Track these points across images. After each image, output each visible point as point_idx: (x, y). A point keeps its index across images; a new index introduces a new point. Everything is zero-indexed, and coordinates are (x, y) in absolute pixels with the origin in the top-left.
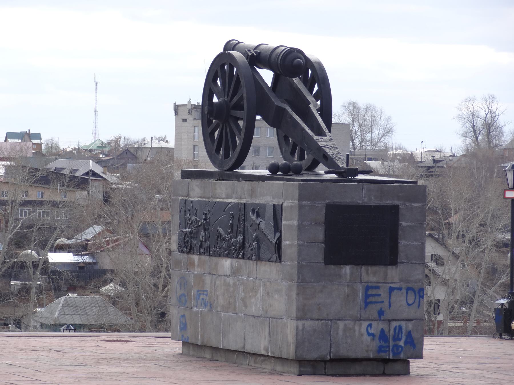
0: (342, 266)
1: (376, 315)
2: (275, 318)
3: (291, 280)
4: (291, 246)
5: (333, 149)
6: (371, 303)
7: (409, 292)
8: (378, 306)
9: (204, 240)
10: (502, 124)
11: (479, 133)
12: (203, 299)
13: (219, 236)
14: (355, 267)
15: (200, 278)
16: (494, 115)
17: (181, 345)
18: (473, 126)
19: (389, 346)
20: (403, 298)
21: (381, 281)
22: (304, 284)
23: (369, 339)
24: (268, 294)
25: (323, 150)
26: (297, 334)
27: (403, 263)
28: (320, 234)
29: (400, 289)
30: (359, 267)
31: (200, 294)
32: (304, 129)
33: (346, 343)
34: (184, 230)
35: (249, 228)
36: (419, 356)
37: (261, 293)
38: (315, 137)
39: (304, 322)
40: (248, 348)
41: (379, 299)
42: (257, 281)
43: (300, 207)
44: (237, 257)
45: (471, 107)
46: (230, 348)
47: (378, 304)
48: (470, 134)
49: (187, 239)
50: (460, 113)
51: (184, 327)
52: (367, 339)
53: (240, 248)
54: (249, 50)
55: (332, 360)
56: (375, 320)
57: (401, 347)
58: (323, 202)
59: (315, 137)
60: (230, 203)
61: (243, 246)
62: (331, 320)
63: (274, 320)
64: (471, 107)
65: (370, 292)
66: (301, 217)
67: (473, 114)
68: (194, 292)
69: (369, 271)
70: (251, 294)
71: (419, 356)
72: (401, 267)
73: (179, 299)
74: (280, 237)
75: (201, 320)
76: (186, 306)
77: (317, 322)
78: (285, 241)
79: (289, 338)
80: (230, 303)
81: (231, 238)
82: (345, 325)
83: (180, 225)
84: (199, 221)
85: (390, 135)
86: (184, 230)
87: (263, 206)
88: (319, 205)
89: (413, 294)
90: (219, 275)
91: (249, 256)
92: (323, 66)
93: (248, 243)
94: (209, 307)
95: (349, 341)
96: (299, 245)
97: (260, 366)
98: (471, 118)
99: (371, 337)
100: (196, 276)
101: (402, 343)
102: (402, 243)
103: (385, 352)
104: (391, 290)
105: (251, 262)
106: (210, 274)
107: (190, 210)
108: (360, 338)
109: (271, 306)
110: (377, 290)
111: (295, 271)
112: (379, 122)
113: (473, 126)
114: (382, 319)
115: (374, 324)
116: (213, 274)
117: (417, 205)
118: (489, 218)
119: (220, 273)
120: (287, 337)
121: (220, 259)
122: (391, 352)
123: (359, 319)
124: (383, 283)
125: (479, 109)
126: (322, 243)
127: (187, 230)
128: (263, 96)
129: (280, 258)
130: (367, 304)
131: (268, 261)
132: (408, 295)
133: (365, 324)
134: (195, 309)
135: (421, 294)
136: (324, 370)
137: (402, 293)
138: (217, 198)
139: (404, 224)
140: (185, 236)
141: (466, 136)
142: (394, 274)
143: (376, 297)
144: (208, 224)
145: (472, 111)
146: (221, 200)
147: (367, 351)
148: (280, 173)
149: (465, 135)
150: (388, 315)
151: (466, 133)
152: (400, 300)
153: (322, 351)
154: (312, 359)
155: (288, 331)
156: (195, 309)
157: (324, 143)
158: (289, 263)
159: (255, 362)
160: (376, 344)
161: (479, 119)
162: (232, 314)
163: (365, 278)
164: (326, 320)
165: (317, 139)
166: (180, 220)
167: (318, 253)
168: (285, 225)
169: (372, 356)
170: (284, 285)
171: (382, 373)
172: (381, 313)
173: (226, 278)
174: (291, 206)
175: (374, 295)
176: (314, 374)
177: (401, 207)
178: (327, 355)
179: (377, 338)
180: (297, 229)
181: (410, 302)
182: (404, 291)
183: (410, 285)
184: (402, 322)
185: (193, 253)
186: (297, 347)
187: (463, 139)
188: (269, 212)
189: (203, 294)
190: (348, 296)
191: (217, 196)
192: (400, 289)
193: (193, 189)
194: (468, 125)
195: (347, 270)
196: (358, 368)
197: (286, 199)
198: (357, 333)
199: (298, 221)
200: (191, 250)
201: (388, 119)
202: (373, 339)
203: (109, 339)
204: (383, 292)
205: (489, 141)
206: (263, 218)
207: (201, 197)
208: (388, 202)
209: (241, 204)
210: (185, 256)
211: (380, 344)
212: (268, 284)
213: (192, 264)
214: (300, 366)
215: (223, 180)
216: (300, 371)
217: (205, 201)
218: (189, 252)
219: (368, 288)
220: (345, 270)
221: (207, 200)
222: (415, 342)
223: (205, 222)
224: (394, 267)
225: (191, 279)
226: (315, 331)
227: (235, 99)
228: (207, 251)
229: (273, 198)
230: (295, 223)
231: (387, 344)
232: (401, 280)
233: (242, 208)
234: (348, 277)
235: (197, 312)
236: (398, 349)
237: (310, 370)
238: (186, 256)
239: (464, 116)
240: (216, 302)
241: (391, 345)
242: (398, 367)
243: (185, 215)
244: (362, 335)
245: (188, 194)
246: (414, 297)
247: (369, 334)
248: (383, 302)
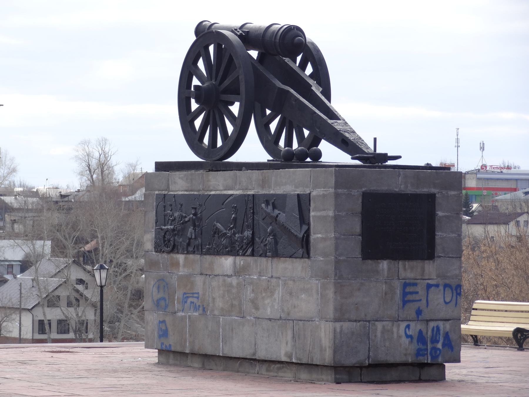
0: (379, 261)
1: (413, 315)
2: (301, 320)
3: (326, 277)
4: (324, 239)
5: (352, 134)
6: (409, 301)
7: (447, 289)
8: (416, 305)
9: (193, 237)
10: (114, 163)
11: (94, 172)
12: (192, 302)
13: (217, 231)
14: (393, 262)
15: (187, 279)
16: (107, 155)
17: (157, 354)
18: (89, 166)
19: (427, 349)
20: (441, 296)
21: (418, 277)
22: (341, 281)
23: (407, 341)
24: (291, 294)
25: (342, 134)
26: (335, 337)
27: (440, 257)
28: (356, 225)
29: (437, 286)
30: (396, 262)
31: (188, 297)
32: (315, 113)
33: (385, 346)
34: (163, 227)
35: (261, 222)
36: (457, 360)
37: (279, 293)
38: (330, 121)
39: (342, 323)
40: (261, 354)
41: (416, 297)
42: (274, 280)
43: (337, 196)
44: (244, 255)
45: (86, 148)
46: (234, 355)
47: (415, 303)
48: (86, 172)
49: (167, 237)
50: (77, 154)
51: (164, 334)
52: (405, 341)
53: (248, 244)
54: (236, 30)
55: (370, 366)
56: (413, 321)
57: (439, 349)
58: (360, 190)
59: (330, 121)
60: (232, 195)
61: (252, 242)
62: (369, 321)
63: (301, 323)
64: (86, 148)
65: (408, 290)
66: (338, 207)
67: (88, 155)
68: (179, 294)
69: (407, 266)
70: (264, 295)
71: (457, 360)
72: (438, 261)
73: (157, 304)
74: (309, 229)
75: (190, 326)
76: (168, 310)
77: (355, 323)
78: (314, 234)
79: (323, 342)
80: (232, 305)
81: (234, 234)
82: (384, 327)
83: (156, 223)
84: (185, 217)
85: (14, 174)
86: (163, 227)
87: (284, 197)
88: (356, 194)
89: (450, 291)
90: (216, 276)
91: (261, 252)
92: (317, 47)
93: (259, 238)
94: (201, 311)
95: (387, 344)
96: (336, 238)
97: (275, 374)
98: (87, 159)
99: (410, 339)
100: (180, 278)
101: (439, 346)
102: (439, 234)
103: (423, 355)
104: (429, 286)
105: (264, 260)
106: (201, 274)
107: (171, 205)
108: (398, 341)
109: (295, 307)
110: (415, 287)
111: (331, 268)
112: (3, 163)
113: (89, 166)
114: (420, 319)
115: (412, 324)
116: (206, 275)
117: (453, 193)
118: (135, 245)
119: (216, 273)
120: (320, 341)
121: (218, 257)
122: (429, 355)
123: (397, 320)
124: (421, 279)
125: (94, 150)
126: (359, 235)
127: (169, 227)
128: (256, 78)
129: (308, 253)
130: (405, 302)
131: (291, 257)
132: (446, 293)
133: (403, 325)
134: (180, 314)
135: (459, 291)
136: (360, 377)
137: (440, 291)
138: (211, 191)
139: (440, 213)
140: (165, 234)
141: (82, 175)
142: (430, 269)
143: (414, 295)
144: (200, 219)
145: (88, 152)
146: (218, 192)
147: (405, 355)
148: (308, 160)
149: (82, 174)
150: (426, 315)
151: (82, 172)
152: (437, 297)
153: (360, 357)
154: (351, 365)
155: (323, 335)
156: (180, 314)
157: (341, 127)
158: (322, 259)
159: (268, 370)
160: (414, 347)
161: (94, 159)
162: (236, 318)
163: (402, 274)
164: (364, 321)
165: (332, 123)
166: (156, 216)
167: (355, 246)
168: (314, 216)
169: (410, 361)
170: (315, 283)
171: (418, 378)
172: (419, 312)
173: (226, 278)
174: (323, 194)
175: (411, 293)
176: (350, 381)
177: (437, 195)
178: (366, 359)
179: (415, 341)
180: (333, 220)
181: (448, 300)
182: (441, 288)
183: (447, 282)
184: (439, 322)
185: (178, 253)
186: (335, 352)
187: (79, 177)
188: (293, 204)
189: (193, 297)
190: (386, 294)
191: (211, 188)
192: (437, 286)
193: (175, 183)
194: (84, 164)
195: (384, 265)
196: (394, 374)
197: (316, 187)
198: (395, 335)
199: (335, 210)
200: (174, 249)
201: (12, 160)
202: (411, 342)
203: (55, 350)
204: (420, 289)
205: (103, 180)
206: (283, 210)
207: (186, 191)
208: (425, 190)
209: (249, 195)
210: (165, 255)
211: (418, 347)
212: (291, 283)
213: (176, 264)
214: (336, 374)
215: (217, 171)
216: (335, 378)
217: (194, 195)
218: (172, 251)
219: (405, 285)
220: (383, 266)
221: (195, 193)
222: (453, 344)
223: (194, 217)
224: (431, 261)
225: (174, 281)
226: (353, 333)
227: (227, 83)
228: (198, 249)
229: (296, 187)
230: (331, 213)
231: (425, 347)
232: (438, 276)
233: (251, 201)
234: (386, 273)
235: (183, 318)
236: (436, 352)
237: (345, 377)
238: (166, 256)
239: (81, 157)
240: (211, 305)
241: (429, 348)
242: (433, 372)
243: (164, 211)
244: (399, 337)
245: (168, 187)
246: (451, 295)
247: (407, 336)
248: (421, 300)
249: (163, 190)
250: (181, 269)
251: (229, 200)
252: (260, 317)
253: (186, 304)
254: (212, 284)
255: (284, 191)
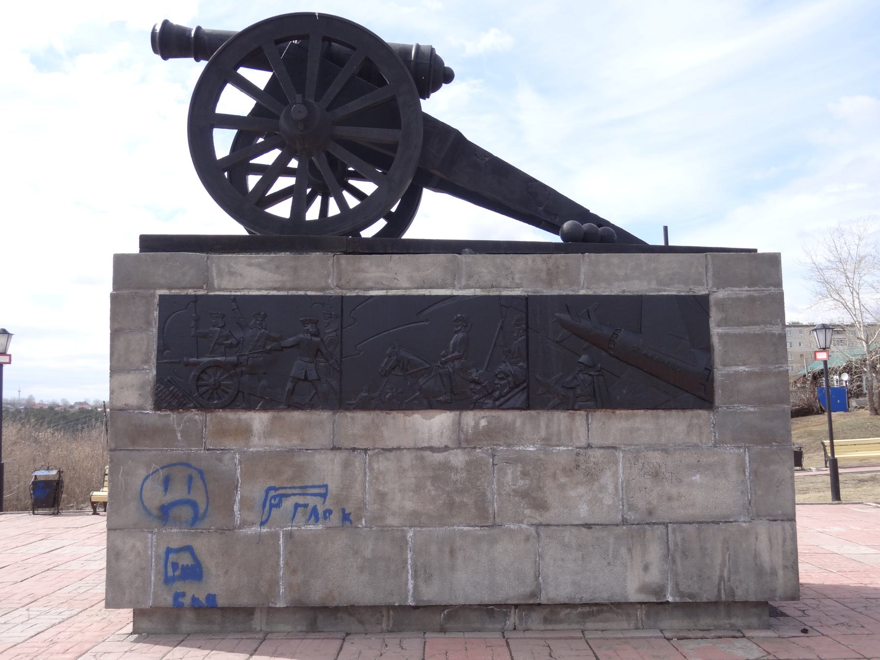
100: (252, 461)
106: (334, 449)
128: (334, 111)
146: (400, 292)
158: (752, 409)
162: (466, 528)
191: (369, 284)
207: (275, 289)
213: (246, 431)
217: (187, 296)
229: (660, 283)
246: (146, 504)
249: (184, 288)
250: (255, 440)
251: (435, 307)
252: (553, 522)
253: (274, 510)
254: (376, 466)
255: (624, 291)
